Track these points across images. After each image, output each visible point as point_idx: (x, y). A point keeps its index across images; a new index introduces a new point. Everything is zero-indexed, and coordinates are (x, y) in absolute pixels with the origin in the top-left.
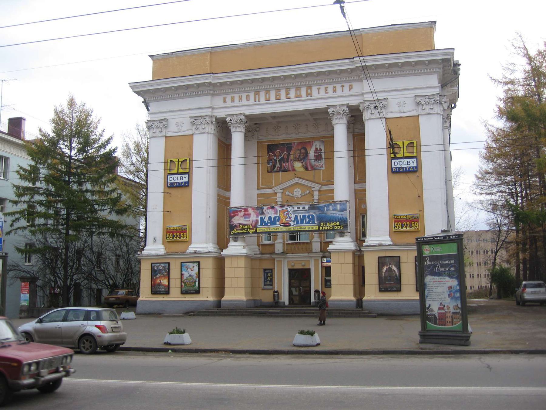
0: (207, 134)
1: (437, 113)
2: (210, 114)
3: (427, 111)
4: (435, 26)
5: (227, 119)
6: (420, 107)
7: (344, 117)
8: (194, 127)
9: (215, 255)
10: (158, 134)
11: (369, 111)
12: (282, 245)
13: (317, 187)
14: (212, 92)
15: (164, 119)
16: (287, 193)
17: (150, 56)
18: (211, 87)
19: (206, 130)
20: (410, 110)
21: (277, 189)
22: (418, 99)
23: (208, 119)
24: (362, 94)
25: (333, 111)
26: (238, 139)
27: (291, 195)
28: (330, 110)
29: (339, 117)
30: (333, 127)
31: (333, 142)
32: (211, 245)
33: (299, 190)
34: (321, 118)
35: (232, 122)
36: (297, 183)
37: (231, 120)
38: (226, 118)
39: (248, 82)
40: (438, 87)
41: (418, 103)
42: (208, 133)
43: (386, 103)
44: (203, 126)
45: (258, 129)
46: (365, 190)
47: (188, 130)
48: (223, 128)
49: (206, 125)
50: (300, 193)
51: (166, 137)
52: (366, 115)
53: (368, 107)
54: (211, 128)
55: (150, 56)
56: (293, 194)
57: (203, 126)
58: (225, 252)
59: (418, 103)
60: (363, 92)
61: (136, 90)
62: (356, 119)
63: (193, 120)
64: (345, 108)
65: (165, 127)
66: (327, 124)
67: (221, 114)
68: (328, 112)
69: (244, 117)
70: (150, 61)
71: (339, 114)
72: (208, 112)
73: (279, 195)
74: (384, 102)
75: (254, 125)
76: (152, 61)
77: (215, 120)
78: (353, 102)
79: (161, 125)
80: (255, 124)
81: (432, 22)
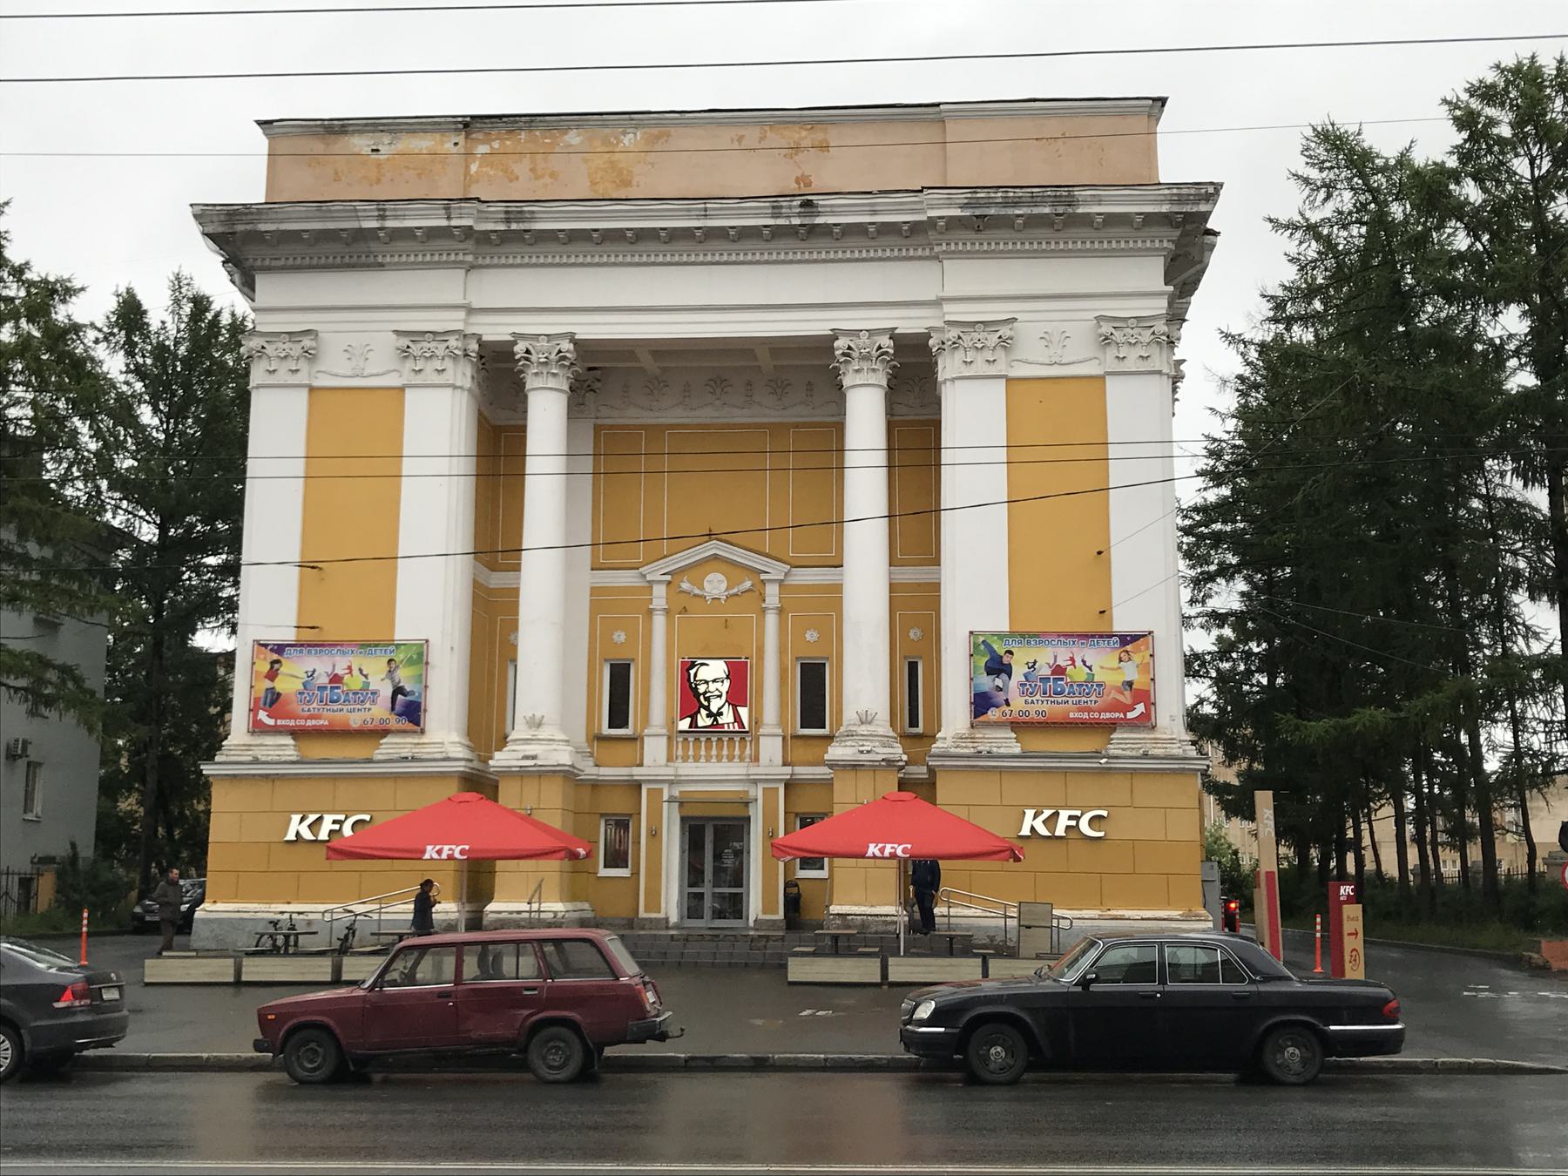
0: (450, 390)
1: (1160, 373)
2: (460, 326)
3: (1131, 364)
4: (1161, 111)
5: (516, 349)
6: (1112, 352)
7: (878, 366)
8: (410, 364)
9: (460, 767)
10: (980, 368)
11: (959, 355)
12: (664, 740)
13: (776, 570)
14: (470, 258)
15: (308, 332)
16: (685, 586)
17: (260, 123)
18: (469, 245)
19: (448, 378)
20: (1081, 359)
21: (656, 571)
22: (1106, 328)
23: (453, 342)
24: (938, 303)
25: (849, 348)
26: (546, 415)
27: (697, 591)
28: (519, 348)
29: (865, 365)
30: (526, 397)
31: (525, 437)
32: (455, 737)
33: (721, 577)
34: (809, 369)
35: (534, 358)
36: (716, 557)
37: (528, 352)
38: (514, 343)
39: (557, 239)
40: (1160, 294)
41: (1107, 340)
42: (455, 387)
43: (1008, 333)
44: (438, 365)
45: (598, 385)
46: (936, 587)
47: (389, 372)
48: (499, 376)
49: (448, 364)
50: (724, 585)
51: (312, 389)
52: (948, 367)
53: (955, 346)
54: (463, 375)
55: (260, 123)
56: (702, 588)
57: (438, 365)
58: (502, 759)
59: (1107, 340)
60: (941, 294)
61: (210, 229)
62: (913, 372)
63: (405, 342)
64: (886, 342)
65: (310, 356)
66: (749, 384)
67: (496, 330)
68: (832, 349)
69: (571, 347)
70: (261, 142)
71: (866, 358)
72: (455, 321)
73: (660, 591)
74: (1005, 331)
75: (598, 372)
76: (266, 141)
77: (476, 347)
78: (910, 323)
79: (296, 350)
80: (590, 369)
81: (1154, 100)
